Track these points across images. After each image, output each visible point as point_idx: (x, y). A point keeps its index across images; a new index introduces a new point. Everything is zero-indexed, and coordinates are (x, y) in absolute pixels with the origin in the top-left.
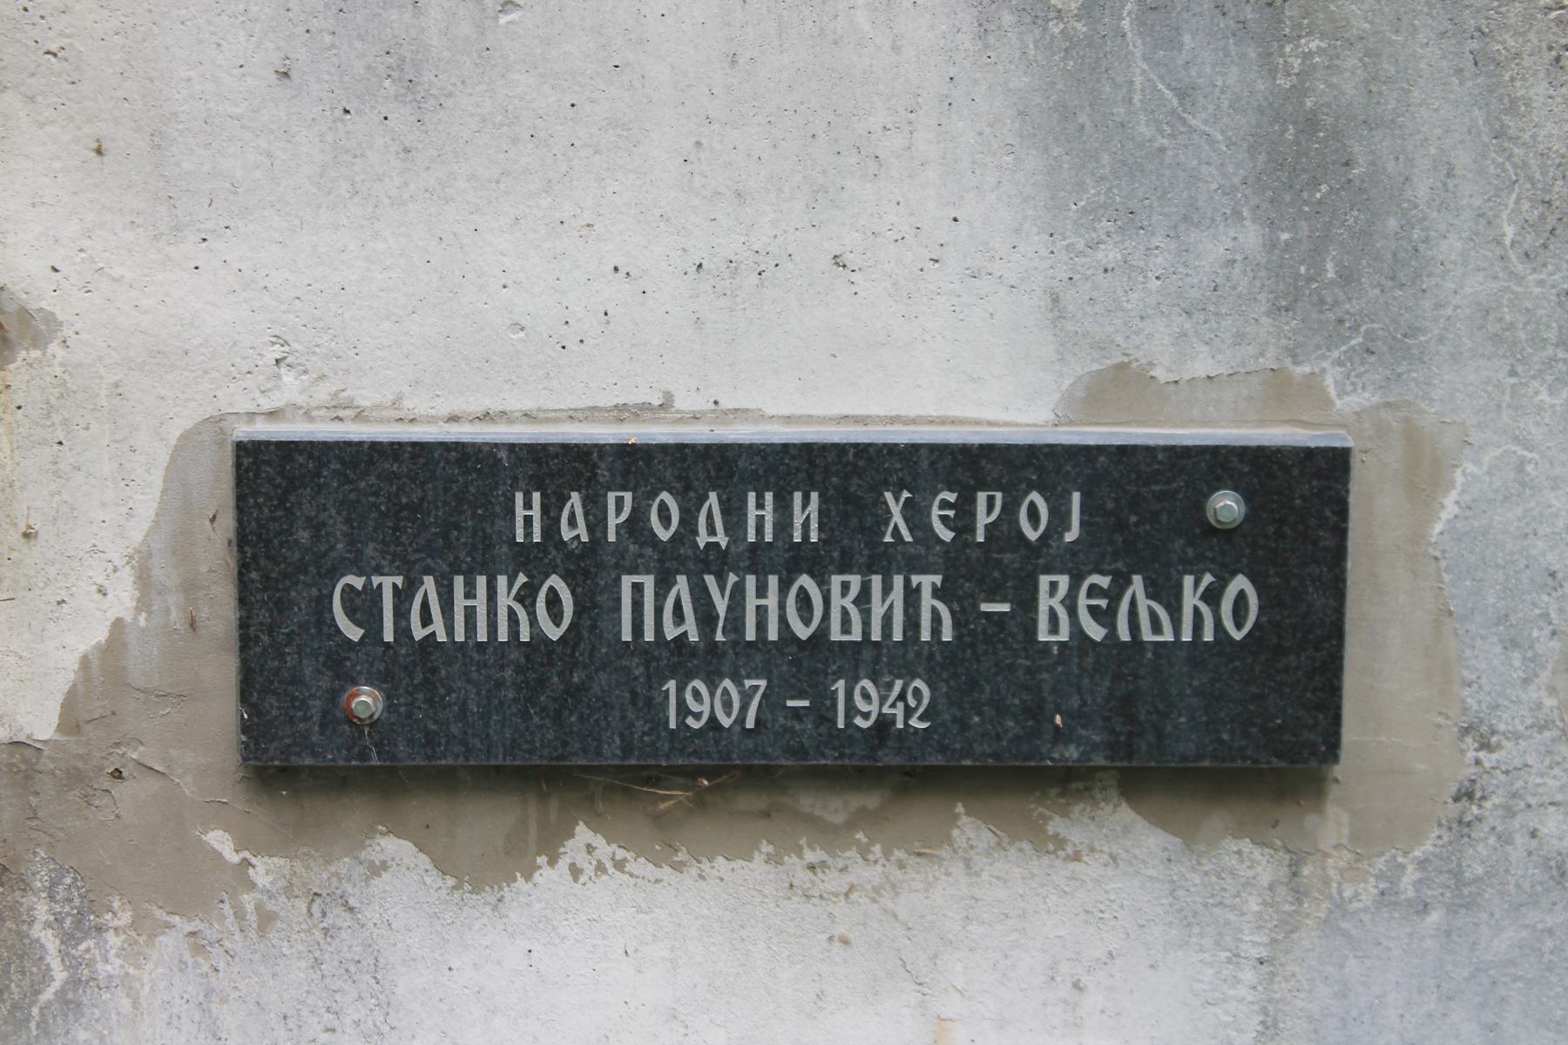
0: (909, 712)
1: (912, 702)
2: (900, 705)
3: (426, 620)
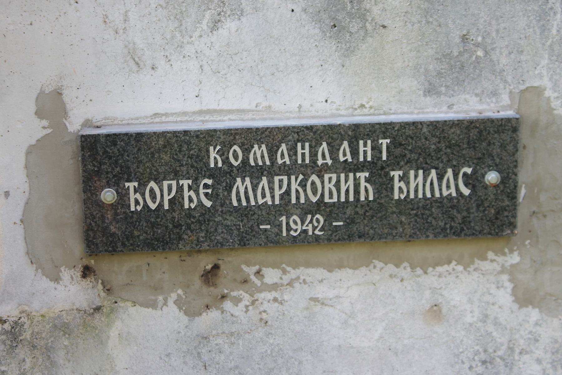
0: (314, 228)
1: (316, 224)
2: (310, 225)
3: (264, 196)
